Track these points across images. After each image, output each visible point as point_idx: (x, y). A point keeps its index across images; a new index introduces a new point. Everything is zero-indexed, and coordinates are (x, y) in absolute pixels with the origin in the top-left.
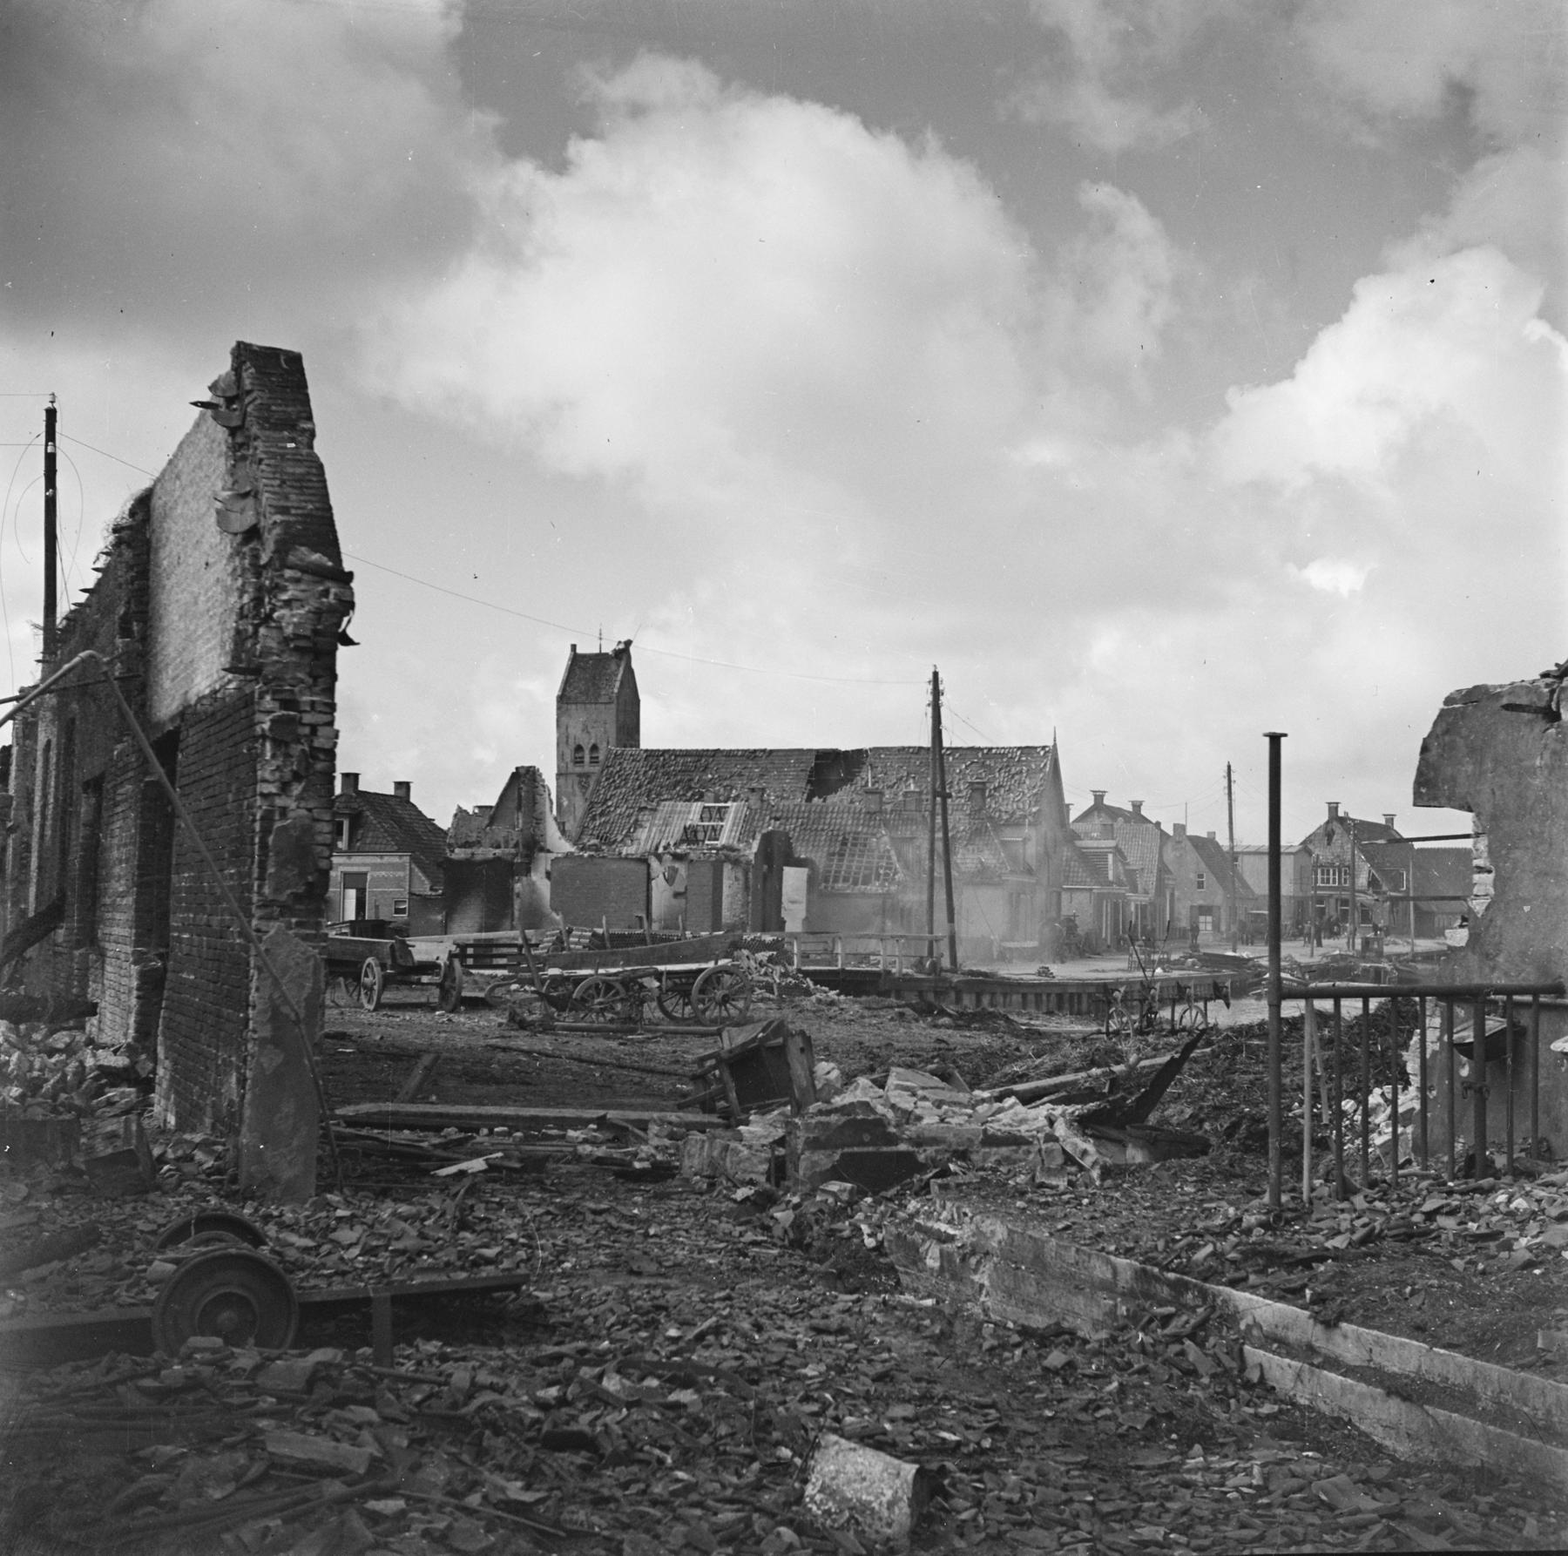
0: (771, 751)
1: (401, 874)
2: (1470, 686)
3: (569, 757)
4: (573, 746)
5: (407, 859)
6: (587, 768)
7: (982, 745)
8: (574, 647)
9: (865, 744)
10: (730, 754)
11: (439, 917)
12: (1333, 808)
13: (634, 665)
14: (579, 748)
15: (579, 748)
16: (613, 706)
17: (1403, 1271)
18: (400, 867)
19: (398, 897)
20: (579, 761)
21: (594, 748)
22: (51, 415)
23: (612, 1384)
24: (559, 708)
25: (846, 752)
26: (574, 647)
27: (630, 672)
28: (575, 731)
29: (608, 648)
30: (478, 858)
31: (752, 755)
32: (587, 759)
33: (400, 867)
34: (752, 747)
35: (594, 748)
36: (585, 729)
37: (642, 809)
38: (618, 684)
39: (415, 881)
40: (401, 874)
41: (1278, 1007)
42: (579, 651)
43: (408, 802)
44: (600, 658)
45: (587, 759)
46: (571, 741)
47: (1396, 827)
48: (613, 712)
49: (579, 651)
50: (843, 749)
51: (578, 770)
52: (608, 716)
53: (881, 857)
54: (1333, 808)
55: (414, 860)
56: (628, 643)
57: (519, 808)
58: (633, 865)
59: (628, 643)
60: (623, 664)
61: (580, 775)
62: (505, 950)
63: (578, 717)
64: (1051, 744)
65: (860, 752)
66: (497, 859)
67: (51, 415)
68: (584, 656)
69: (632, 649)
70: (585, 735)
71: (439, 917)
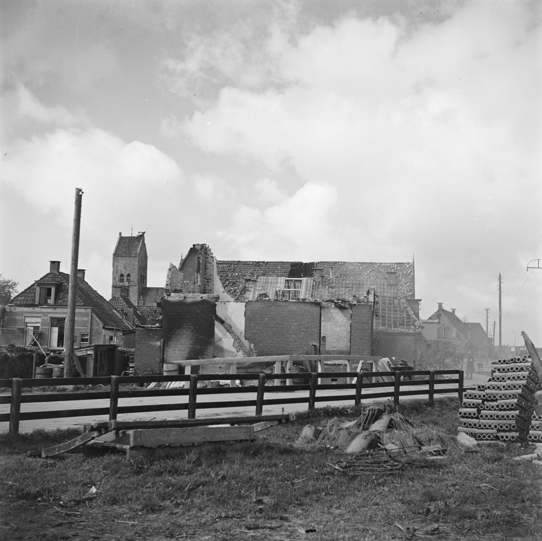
0: (267, 262)
1: (86, 319)
3: (117, 279)
4: (119, 274)
5: (89, 310)
7: (376, 262)
8: (120, 234)
9: (316, 260)
11: (158, 344)
12: (440, 305)
13: (146, 242)
14: (122, 275)
15: (122, 275)
16: (137, 258)
18: (86, 315)
19: (84, 332)
20: (122, 280)
21: (129, 275)
23: (10, 496)
24: (114, 259)
25: (306, 264)
26: (120, 234)
27: (144, 244)
28: (121, 268)
29: (135, 234)
30: (189, 300)
32: (125, 280)
33: (86, 315)
34: (257, 260)
35: (129, 275)
36: (125, 268)
37: (247, 280)
38: (139, 249)
39: (94, 323)
40: (86, 319)
41: (361, 391)
42: (122, 235)
43: (84, 280)
44: (131, 239)
45: (125, 280)
46: (119, 272)
47: (456, 314)
48: (137, 260)
49: (122, 235)
50: (304, 262)
52: (135, 262)
53: (402, 311)
54: (440, 305)
55: (93, 311)
56: (144, 233)
57: (198, 271)
58: (308, 307)
59: (144, 233)
62: (446, 377)
63: (122, 262)
64: (412, 262)
65: (312, 264)
66: (204, 302)
69: (145, 235)
70: (125, 270)
71: (158, 344)
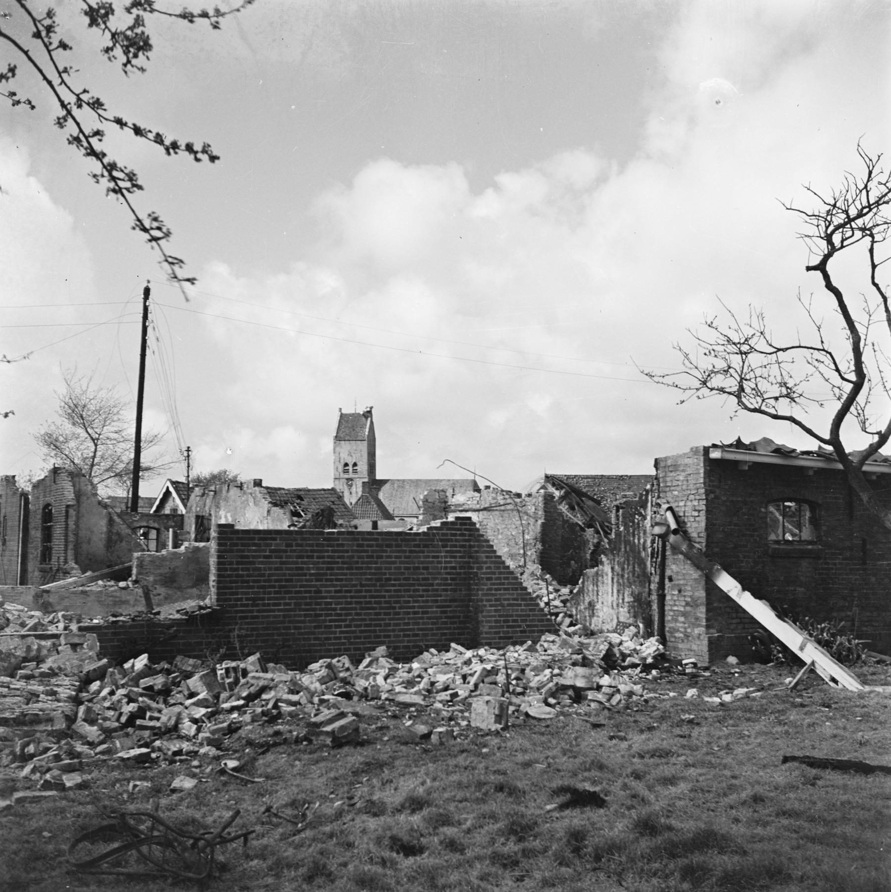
2: (757, 601)
3: (341, 468)
4: (343, 463)
6: (351, 475)
10: (609, 478)
14: (346, 465)
15: (346, 465)
17: (717, 802)
20: (346, 471)
21: (355, 465)
22: (147, 292)
29: (361, 411)
31: (621, 478)
36: (350, 454)
42: (343, 412)
44: (356, 416)
51: (346, 476)
56: (371, 408)
59: (371, 408)
60: (369, 419)
61: (347, 479)
63: (346, 447)
67: (147, 292)
68: (346, 415)
